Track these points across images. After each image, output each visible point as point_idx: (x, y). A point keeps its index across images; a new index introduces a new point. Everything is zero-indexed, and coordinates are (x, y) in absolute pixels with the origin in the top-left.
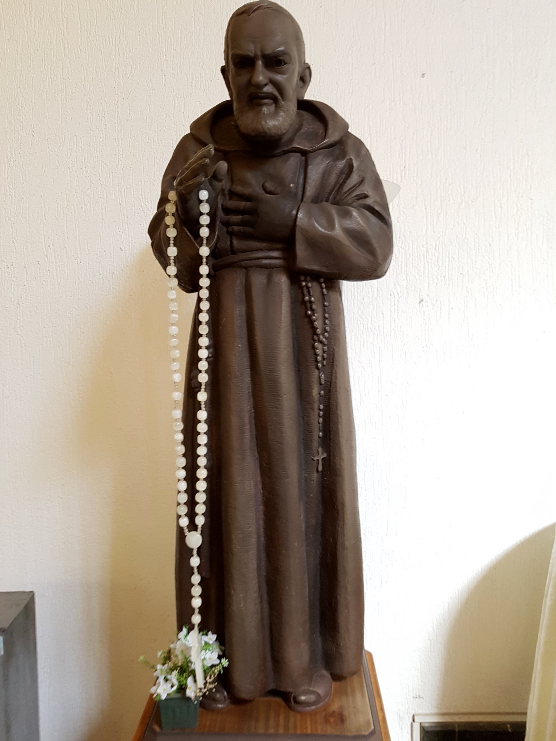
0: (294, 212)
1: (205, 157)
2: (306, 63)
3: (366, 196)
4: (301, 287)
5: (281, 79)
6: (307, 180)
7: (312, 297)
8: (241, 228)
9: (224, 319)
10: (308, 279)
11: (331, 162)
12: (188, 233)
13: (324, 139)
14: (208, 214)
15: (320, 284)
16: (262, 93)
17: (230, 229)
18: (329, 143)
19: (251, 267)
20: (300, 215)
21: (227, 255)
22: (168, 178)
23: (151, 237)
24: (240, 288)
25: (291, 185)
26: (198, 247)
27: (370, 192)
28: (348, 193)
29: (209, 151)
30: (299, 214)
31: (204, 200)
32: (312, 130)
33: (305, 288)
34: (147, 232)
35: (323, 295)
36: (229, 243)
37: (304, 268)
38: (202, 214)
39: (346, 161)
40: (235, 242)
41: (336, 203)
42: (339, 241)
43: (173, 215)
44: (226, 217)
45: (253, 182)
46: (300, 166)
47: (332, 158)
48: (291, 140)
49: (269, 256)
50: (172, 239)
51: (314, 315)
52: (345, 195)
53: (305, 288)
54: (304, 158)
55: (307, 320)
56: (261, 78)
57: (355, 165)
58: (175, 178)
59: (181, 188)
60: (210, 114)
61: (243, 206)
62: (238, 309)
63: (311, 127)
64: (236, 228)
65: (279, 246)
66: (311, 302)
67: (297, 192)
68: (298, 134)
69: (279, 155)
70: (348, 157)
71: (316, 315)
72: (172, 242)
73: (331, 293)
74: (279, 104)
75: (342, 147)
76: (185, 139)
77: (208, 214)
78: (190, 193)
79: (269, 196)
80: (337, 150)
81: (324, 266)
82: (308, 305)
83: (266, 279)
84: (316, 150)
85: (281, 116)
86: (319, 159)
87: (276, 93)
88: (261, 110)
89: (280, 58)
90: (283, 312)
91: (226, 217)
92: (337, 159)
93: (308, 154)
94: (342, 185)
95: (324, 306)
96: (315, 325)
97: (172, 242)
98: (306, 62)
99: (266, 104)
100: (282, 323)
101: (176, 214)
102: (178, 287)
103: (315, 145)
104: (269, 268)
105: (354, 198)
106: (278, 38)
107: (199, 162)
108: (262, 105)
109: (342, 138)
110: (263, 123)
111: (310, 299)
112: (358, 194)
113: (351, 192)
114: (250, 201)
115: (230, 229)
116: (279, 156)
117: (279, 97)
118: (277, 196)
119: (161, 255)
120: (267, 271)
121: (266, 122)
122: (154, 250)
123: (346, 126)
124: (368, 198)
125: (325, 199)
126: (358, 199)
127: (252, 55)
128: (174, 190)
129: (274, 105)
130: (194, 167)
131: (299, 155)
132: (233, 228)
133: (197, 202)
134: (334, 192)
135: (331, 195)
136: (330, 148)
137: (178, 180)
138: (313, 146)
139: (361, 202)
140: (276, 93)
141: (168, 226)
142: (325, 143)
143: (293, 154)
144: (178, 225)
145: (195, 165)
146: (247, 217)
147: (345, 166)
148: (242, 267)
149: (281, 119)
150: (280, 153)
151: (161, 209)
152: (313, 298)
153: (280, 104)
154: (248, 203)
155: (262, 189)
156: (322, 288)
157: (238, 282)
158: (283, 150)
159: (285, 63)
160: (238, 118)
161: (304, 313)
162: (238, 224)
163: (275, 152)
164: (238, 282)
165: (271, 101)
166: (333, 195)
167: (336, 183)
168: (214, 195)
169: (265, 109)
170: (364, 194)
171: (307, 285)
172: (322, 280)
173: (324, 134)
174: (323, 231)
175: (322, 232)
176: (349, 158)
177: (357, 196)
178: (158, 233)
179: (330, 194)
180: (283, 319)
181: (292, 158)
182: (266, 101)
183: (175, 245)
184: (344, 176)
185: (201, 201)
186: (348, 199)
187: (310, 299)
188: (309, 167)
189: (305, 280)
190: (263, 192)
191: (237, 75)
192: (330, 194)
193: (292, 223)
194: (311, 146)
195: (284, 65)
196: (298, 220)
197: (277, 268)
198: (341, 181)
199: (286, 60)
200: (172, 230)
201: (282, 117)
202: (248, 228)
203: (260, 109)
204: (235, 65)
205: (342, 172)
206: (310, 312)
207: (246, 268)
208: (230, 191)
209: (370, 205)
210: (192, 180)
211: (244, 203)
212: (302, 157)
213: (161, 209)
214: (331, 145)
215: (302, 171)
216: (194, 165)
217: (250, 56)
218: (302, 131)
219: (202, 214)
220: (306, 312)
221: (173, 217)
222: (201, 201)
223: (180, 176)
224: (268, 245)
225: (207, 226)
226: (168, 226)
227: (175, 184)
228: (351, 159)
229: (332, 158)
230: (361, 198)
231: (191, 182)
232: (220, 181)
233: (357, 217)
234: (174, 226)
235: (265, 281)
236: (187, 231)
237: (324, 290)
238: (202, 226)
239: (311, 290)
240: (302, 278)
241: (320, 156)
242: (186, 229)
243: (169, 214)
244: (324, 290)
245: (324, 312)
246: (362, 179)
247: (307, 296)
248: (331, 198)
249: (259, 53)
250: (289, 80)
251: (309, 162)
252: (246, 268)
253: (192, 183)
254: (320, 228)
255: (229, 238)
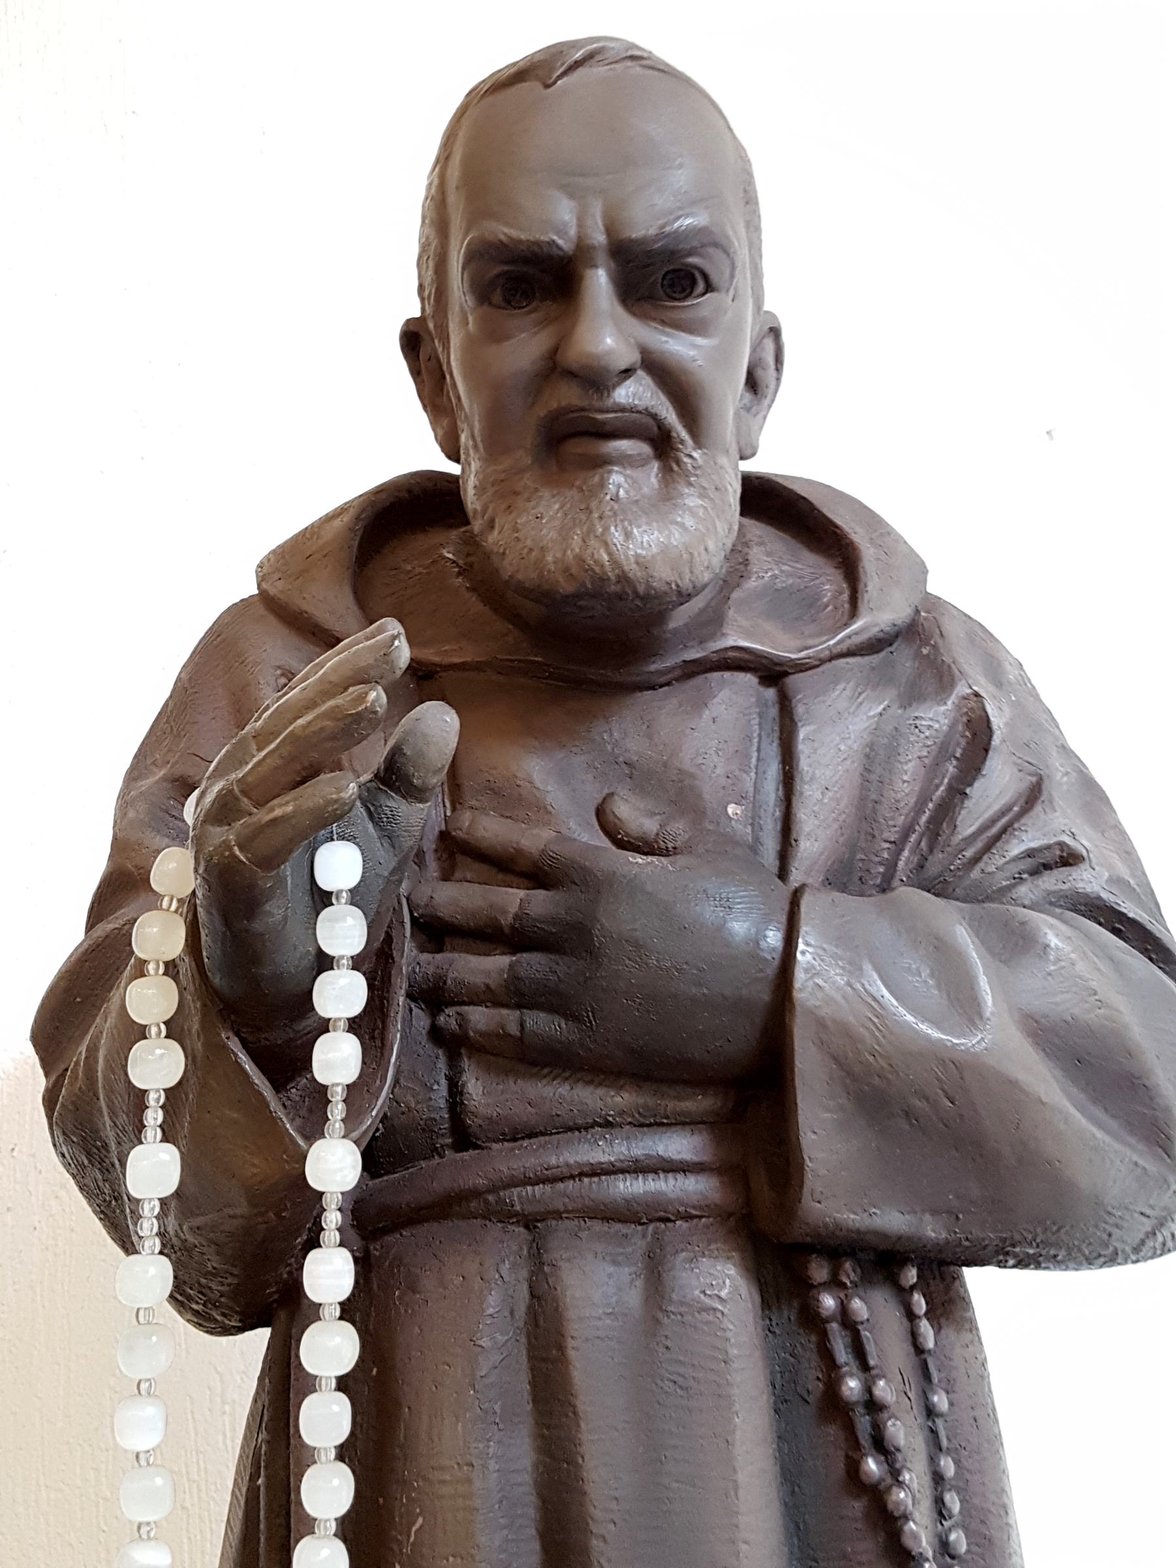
0: (774, 938)
1: (362, 678)
2: (767, 312)
3: (1069, 859)
4: (812, 1320)
5: (692, 353)
6: (798, 786)
7: (879, 1377)
8: (510, 1018)
9: (420, 1520)
10: (849, 1272)
11: (895, 706)
12: (248, 1066)
13: (854, 613)
14: (357, 963)
15: (903, 1295)
16: (608, 412)
17: (448, 1019)
18: (875, 630)
19: (558, 1215)
20: (804, 955)
21: (436, 1151)
22: (146, 783)
23: (47, 1064)
24: (501, 1338)
25: (731, 809)
26: (301, 1142)
27: (1084, 840)
28: (979, 844)
29: (386, 653)
30: (801, 946)
31: (340, 892)
32: (790, 581)
33: (834, 1326)
34: (28, 1034)
35: (919, 1349)
36: (442, 1089)
37: (838, 1226)
38: (324, 962)
39: (958, 707)
40: (474, 1087)
41: (939, 888)
42: (1014, 1084)
43: (171, 969)
44: (430, 962)
45: (554, 794)
46: (760, 724)
47: (893, 693)
48: (713, 620)
49: (648, 1156)
50: (155, 1100)
51: (900, 1484)
52: (969, 853)
53: (834, 1326)
54: (771, 693)
55: (857, 1507)
56: (609, 341)
57: (998, 720)
58: (185, 787)
59: (219, 834)
60: (352, 513)
61: (513, 909)
62: (493, 1465)
63: (785, 568)
64: (480, 1017)
65: (698, 1103)
66: (873, 1406)
67: (757, 839)
68: (736, 595)
69: (663, 680)
70: (962, 689)
71: (906, 1476)
72: (154, 1117)
73: (949, 1333)
74: (678, 462)
75: (925, 651)
76: (238, 612)
77: (357, 963)
78: (271, 861)
79: (640, 859)
80: (903, 658)
81: (935, 1212)
82: (863, 1423)
83: (639, 1283)
84: (823, 662)
85: (690, 509)
86: (839, 696)
87: (669, 415)
88: (602, 485)
89: (692, 260)
90: (741, 1477)
91: (430, 962)
92: (912, 696)
93: (787, 674)
94: (947, 810)
95: (930, 1412)
96: (908, 1542)
97: (154, 1117)
98: (766, 307)
99: (625, 461)
100: (744, 1547)
101: (186, 968)
102: (170, 1313)
103: (816, 641)
104: (651, 1221)
105: (1014, 869)
106: (681, 178)
107: (331, 703)
108: (602, 462)
109: (917, 612)
110: (616, 536)
111: (868, 1389)
112: (1034, 845)
113: (997, 838)
114: (544, 886)
115: (448, 1019)
116: (661, 686)
117: (680, 431)
118: (681, 860)
119: (89, 1154)
120: (638, 1240)
121: (628, 535)
122: (57, 1132)
123: (921, 570)
124: (1084, 866)
125: (881, 869)
126: (1035, 872)
127: (565, 244)
128: (182, 844)
129: (655, 466)
130: (304, 727)
131: (749, 680)
132: (463, 1020)
133: (304, 900)
134: (913, 838)
135: (902, 850)
136: (877, 652)
137: (210, 798)
138: (810, 642)
139: (1051, 882)
140: (669, 415)
141: (141, 1033)
142: (856, 633)
143: (727, 675)
144: (194, 1024)
145: (309, 717)
146: (534, 963)
147: (952, 727)
148: (506, 1215)
149: (689, 522)
150: (673, 668)
151: (105, 927)
152: (882, 1383)
153: (686, 460)
154: (541, 893)
155: (597, 827)
156: (911, 1316)
157: (493, 1302)
158: (682, 658)
159: (709, 288)
160: (491, 525)
161: (840, 1466)
162: (488, 997)
163: (646, 669)
164: (493, 1302)
165: (644, 448)
166: (913, 852)
167: (919, 809)
168: (387, 860)
169: (617, 479)
170: (1062, 845)
171: (844, 1309)
172: (911, 1275)
173: (846, 596)
174: (935, 1034)
175: (928, 1038)
176: (969, 691)
177: (1030, 854)
178: (83, 1048)
179: (898, 846)
180: (742, 1520)
181: (724, 695)
182: (624, 445)
183: (167, 1137)
184: (951, 768)
185: (323, 899)
186: (992, 869)
187: (868, 1389)
188: (802, 734)
189: (835, 1283)
190: (604, 842)
191: (493, 335)
192: (898, 846)
193: (763, 995)
194: (799, 643)
195: (703, 294)
196: (800, 977)
197: (688, 1217)
198: (942, 788)
199: (714, 277)
200: (159, 1052)
201: (694, 514)
202: (543, 1016)
203: (596, 479)
204: (483, 292)
205: (943, 751)
206: (877, 1462)
207: (529, 1222)
208: (445, 837)
209: (1099, 898)
210: (288, 797)
211: (522, 893)
212: (762, 689)
213: (105, 927)
214: (879, 640)
215: (772, 751)
216: (300, 722)
217: (559, 247)
218: (752, 584)
219: (324, 962)
220: (853, 1469)
221: (170, 983)
222: (323, 899)
223: (218, 773)
224: (641, 1101)
225: (354, 1026)
226: (141, 1033)
227: (189, 812)
228: (977, 695)
229: (893, 693)
230: (1047, 867)
231: (283, 807)
232: (414, 793)
233: (1073, 956)
234: (174, 1029)
235: (634, 1297)
236: (243, 1058)
237: (926, 1328)
238: (324, 1026)
239: (865, 1333)
240: (819, 1272)
241: (840, 687)
242: (234, 1045)
243: (151, 967)
244: (926, 1328)
245: (935, 1445)
246: (1034, 779)
247: (852, 1375)
248: (901, 864)
249: (599, 238)
250: (724, 355)
251: (800, 710)
252: (529, 1222)
253: (290, 808)
254: (909, 1018)
255: (442, 1064)
